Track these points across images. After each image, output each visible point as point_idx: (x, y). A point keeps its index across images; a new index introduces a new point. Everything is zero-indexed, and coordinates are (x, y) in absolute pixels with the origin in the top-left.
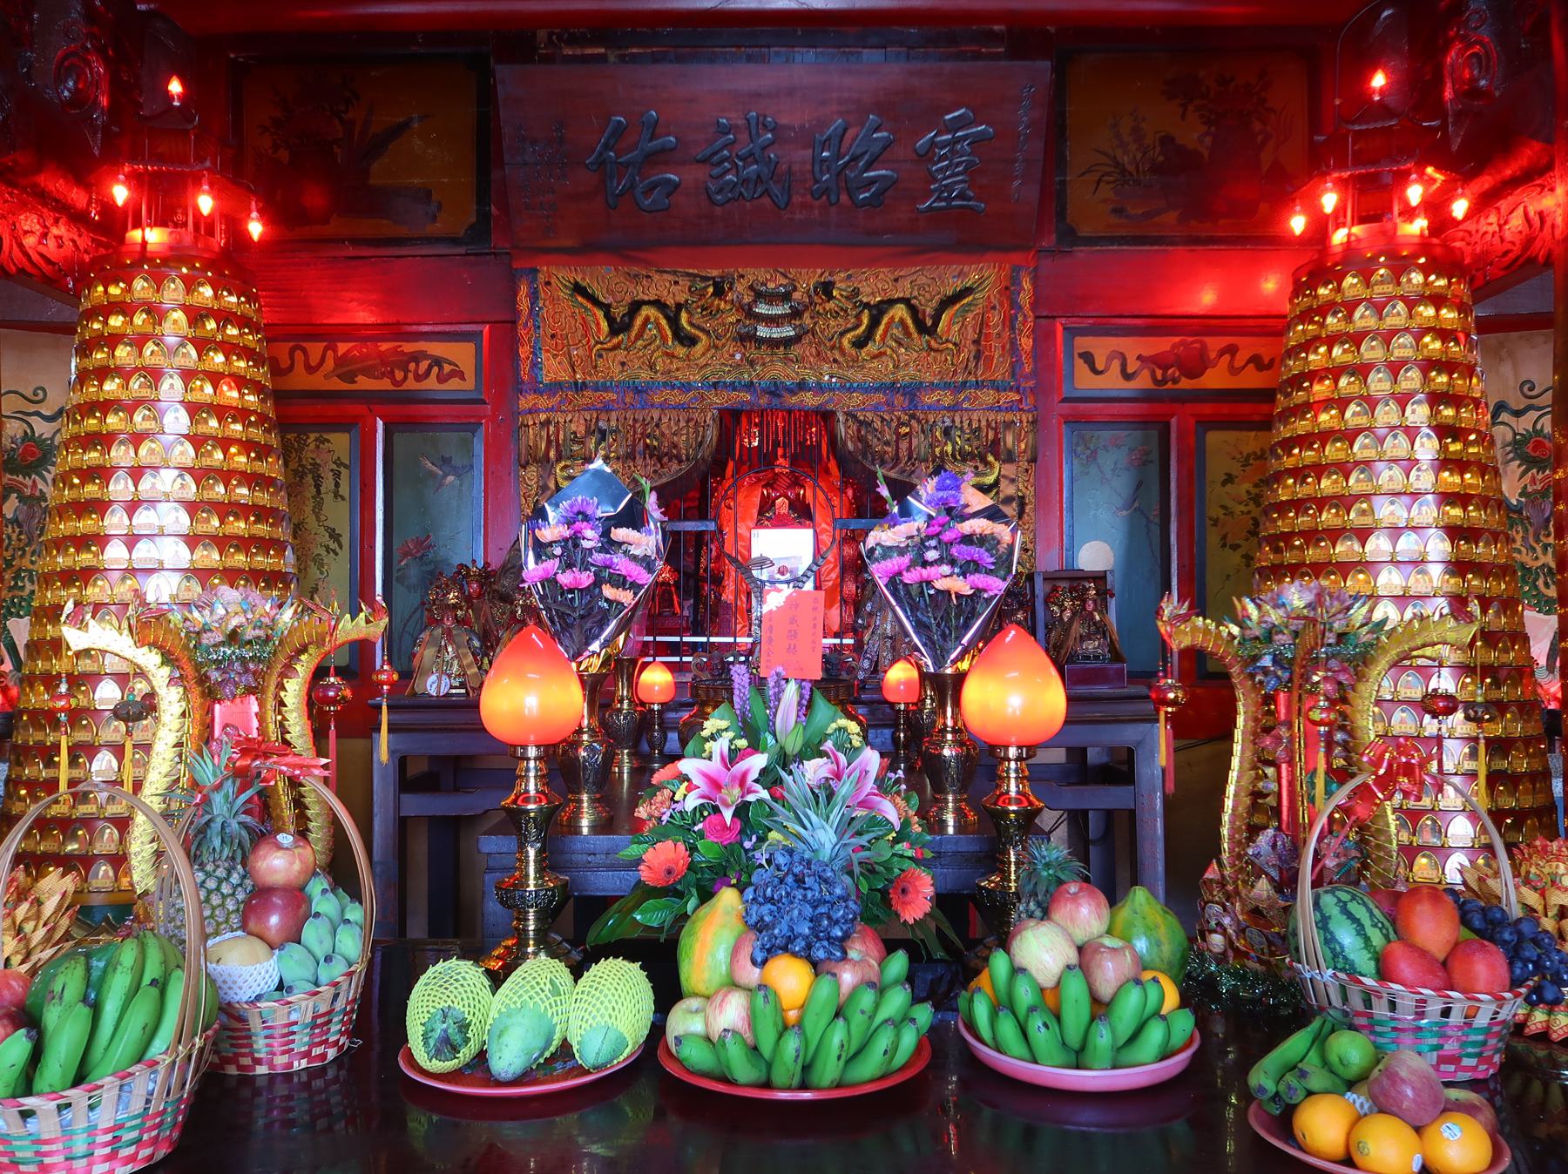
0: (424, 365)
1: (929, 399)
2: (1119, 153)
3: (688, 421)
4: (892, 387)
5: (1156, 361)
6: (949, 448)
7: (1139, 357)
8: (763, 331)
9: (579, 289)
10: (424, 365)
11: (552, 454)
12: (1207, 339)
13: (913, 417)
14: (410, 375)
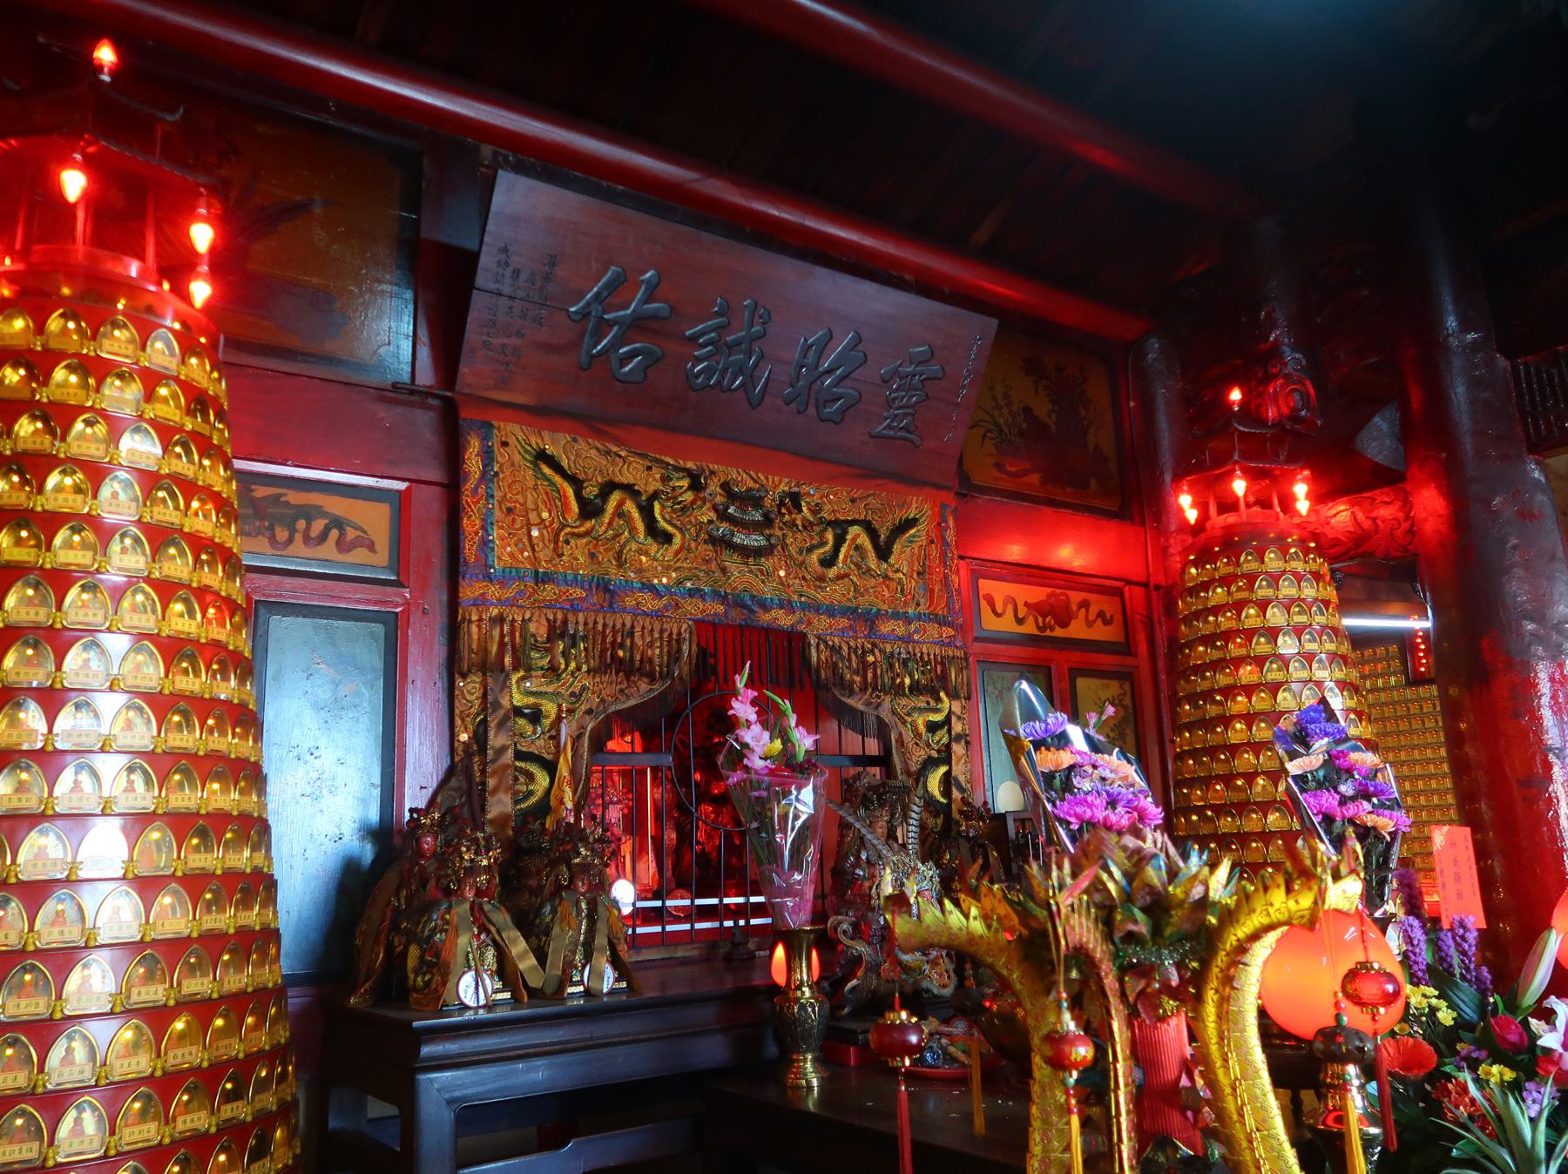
0: (318, 526)
1: (886, 628)
2: (996, 413)
3: (662, 632)
4: (850, 612)
5: (1036, 608)
6: (907, 681)
7: (1026, 604)
8: (739, 538)
9: (542, 456)
10: (318, 526)
11: (508, 660)
12: (1069, 593)
13: (874, 645)
14: (298, 537)
